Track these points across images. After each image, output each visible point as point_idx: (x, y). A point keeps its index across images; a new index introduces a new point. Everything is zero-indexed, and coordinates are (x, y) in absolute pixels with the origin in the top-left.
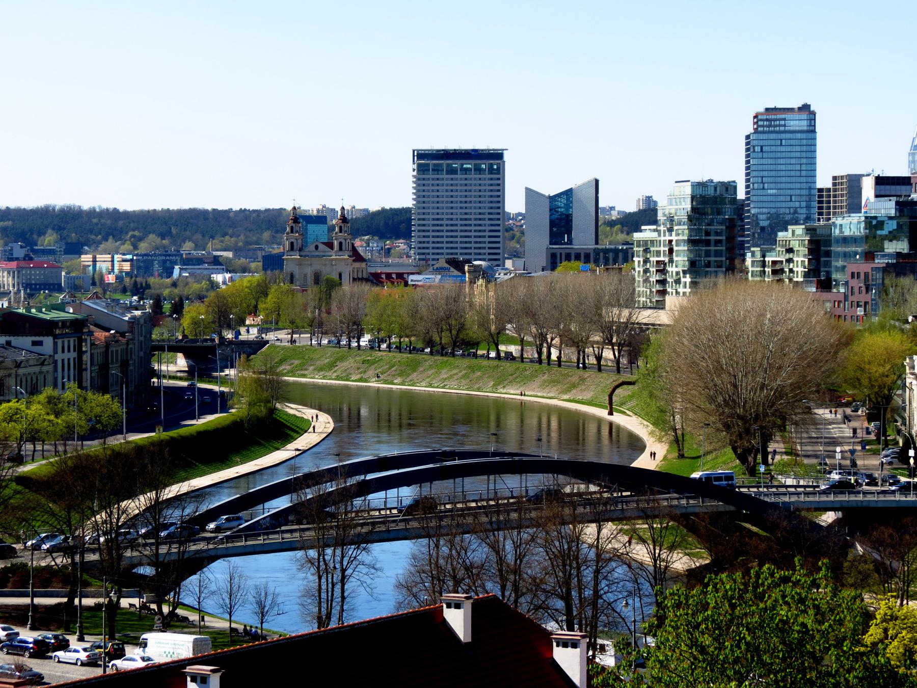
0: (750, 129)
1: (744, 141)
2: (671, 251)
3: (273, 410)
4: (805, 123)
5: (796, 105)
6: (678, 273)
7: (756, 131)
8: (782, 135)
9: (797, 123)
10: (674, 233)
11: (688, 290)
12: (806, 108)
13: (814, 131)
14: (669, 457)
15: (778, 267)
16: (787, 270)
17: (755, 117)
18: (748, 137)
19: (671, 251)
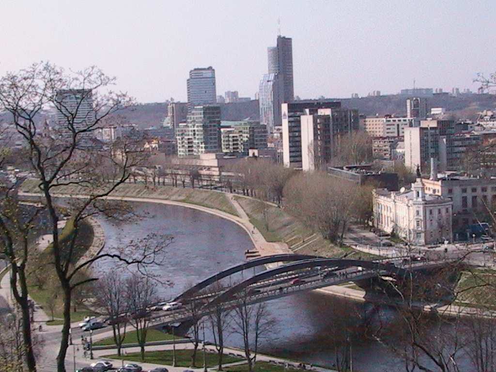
0: (188, 77)
1: (186, 82)
2: (194, 134)
3: (198, 172)
4: (211, 74)
5: (206, 67)
6: (198, 143)
7: (191, 78)
8: (202, 79)
9: (208, 74)
10: (195, 127)
11: (203, 150)
12: (210, 68)
13: (214, 77)
14: (409, 92)
15: (235, 138)
16: (240, 139)
17: (190, 72)
18: (188, 80)
19: (194, 134)
